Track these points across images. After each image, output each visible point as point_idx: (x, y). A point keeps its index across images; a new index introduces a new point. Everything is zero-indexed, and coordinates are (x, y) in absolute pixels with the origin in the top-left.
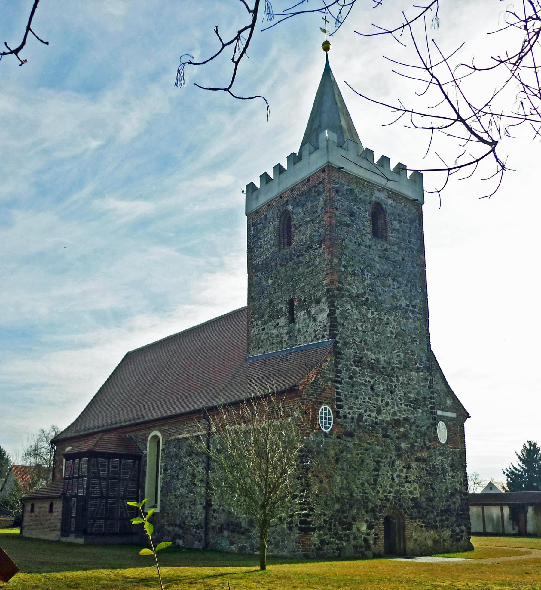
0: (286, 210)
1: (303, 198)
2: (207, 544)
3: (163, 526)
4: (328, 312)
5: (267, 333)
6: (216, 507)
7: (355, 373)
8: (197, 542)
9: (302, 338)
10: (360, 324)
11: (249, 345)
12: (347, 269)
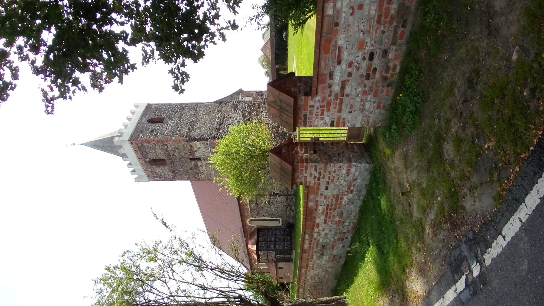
0: (148, 162)
1: (144, 153)
2: (294, 195)
4: (196, 142)
5: (205, 171)
6: (279, 191)
8: (293, 200)
9: (207, 154)
10: (202, 129)
11: (209, 180)
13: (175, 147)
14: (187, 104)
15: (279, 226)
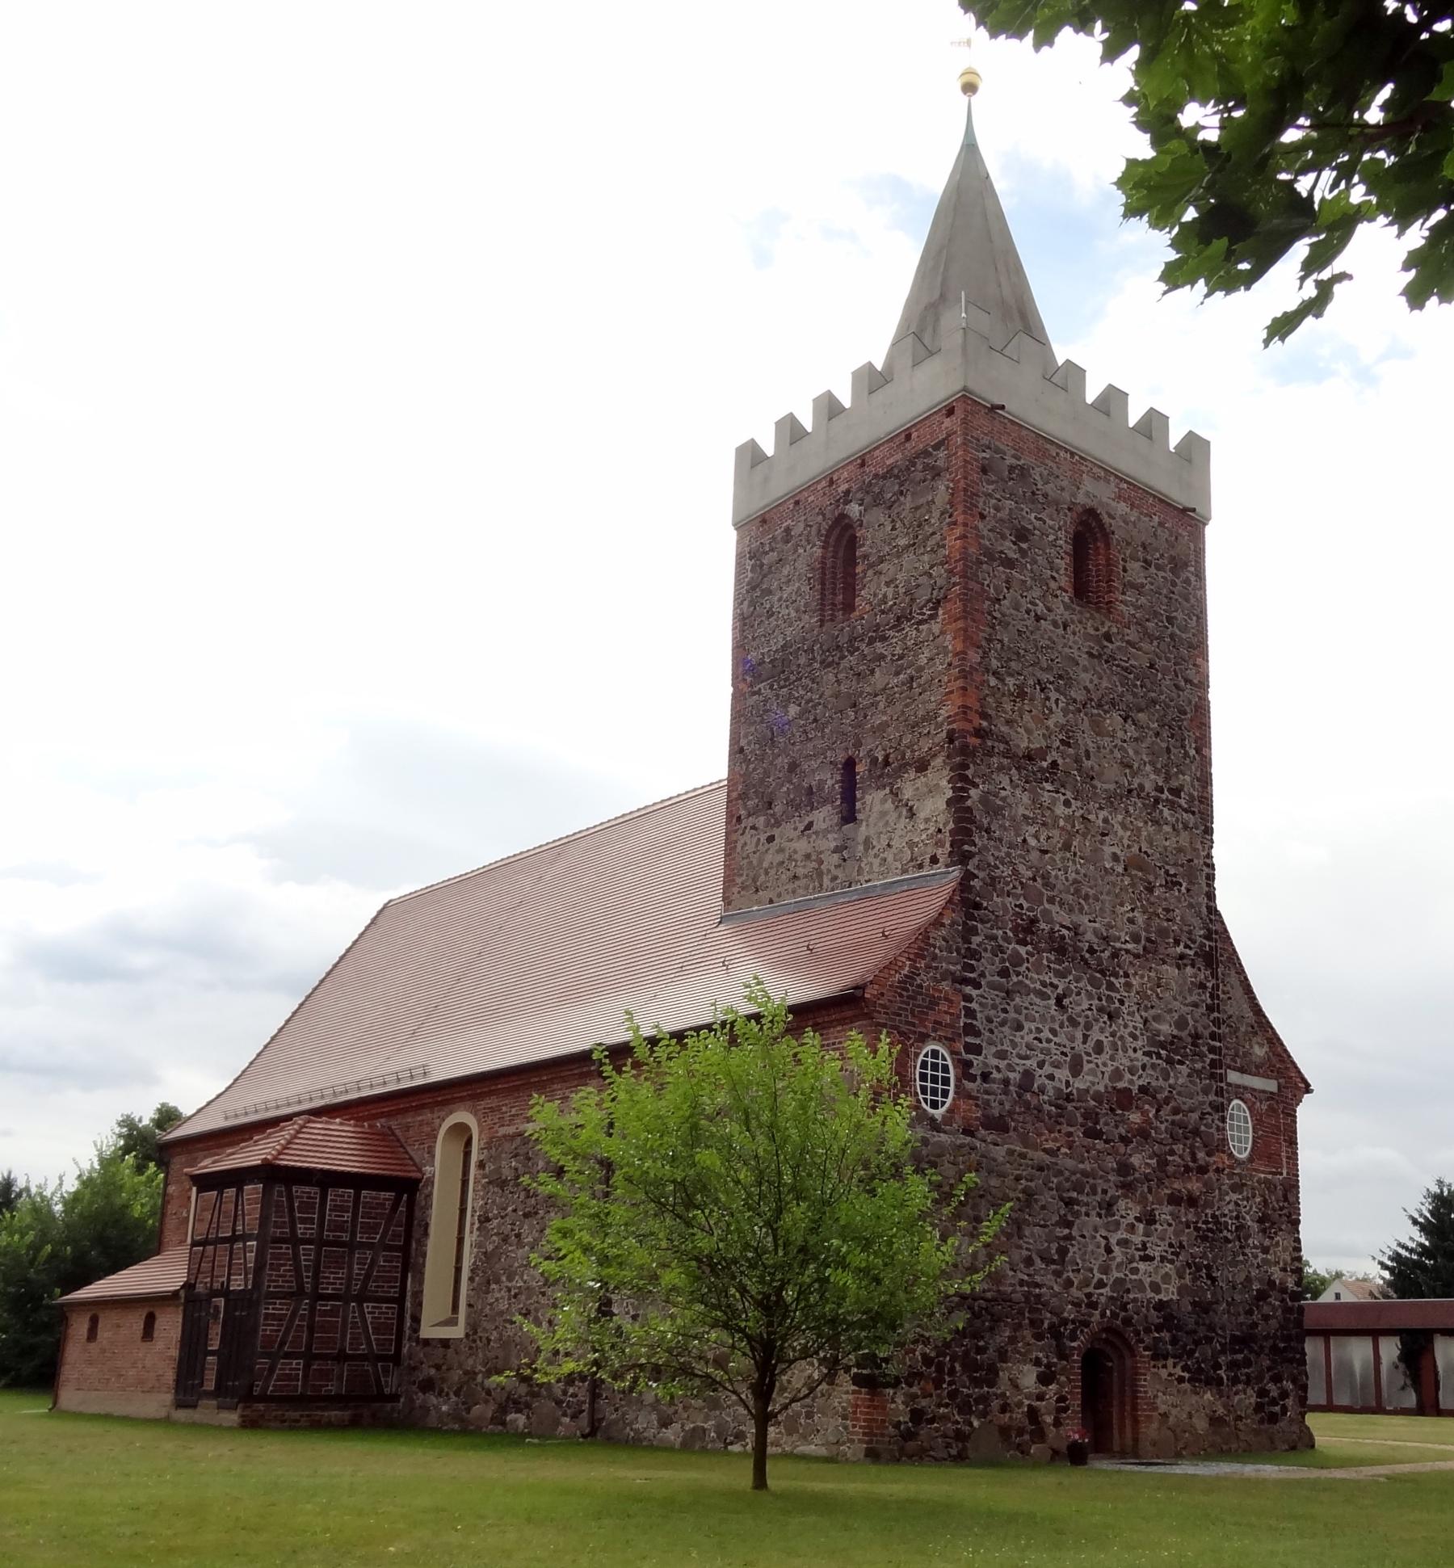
0: (843, 516)
1: (892, 487)
3: (471, 1374)
4: (950, 794)
5: (781, 850)
7: (1017, 960)
9: (876, 862)
10: (1032, 830)
12: (1002, 681)
13: (920, 669)
14: (1198, 750)
15: (416, 1320)
